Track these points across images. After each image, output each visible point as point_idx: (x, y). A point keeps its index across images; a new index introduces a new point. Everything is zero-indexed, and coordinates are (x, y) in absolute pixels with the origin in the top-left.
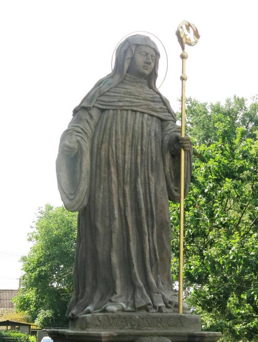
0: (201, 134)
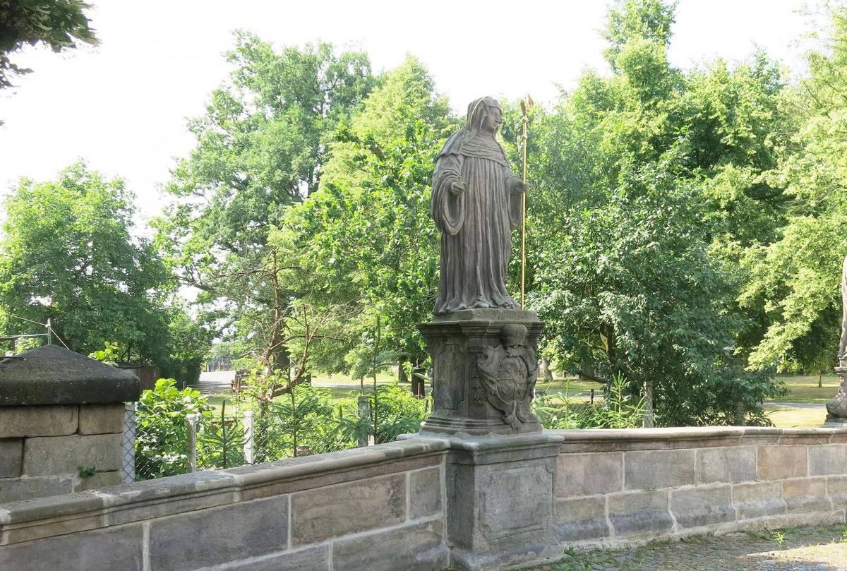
0: (266, 89)
